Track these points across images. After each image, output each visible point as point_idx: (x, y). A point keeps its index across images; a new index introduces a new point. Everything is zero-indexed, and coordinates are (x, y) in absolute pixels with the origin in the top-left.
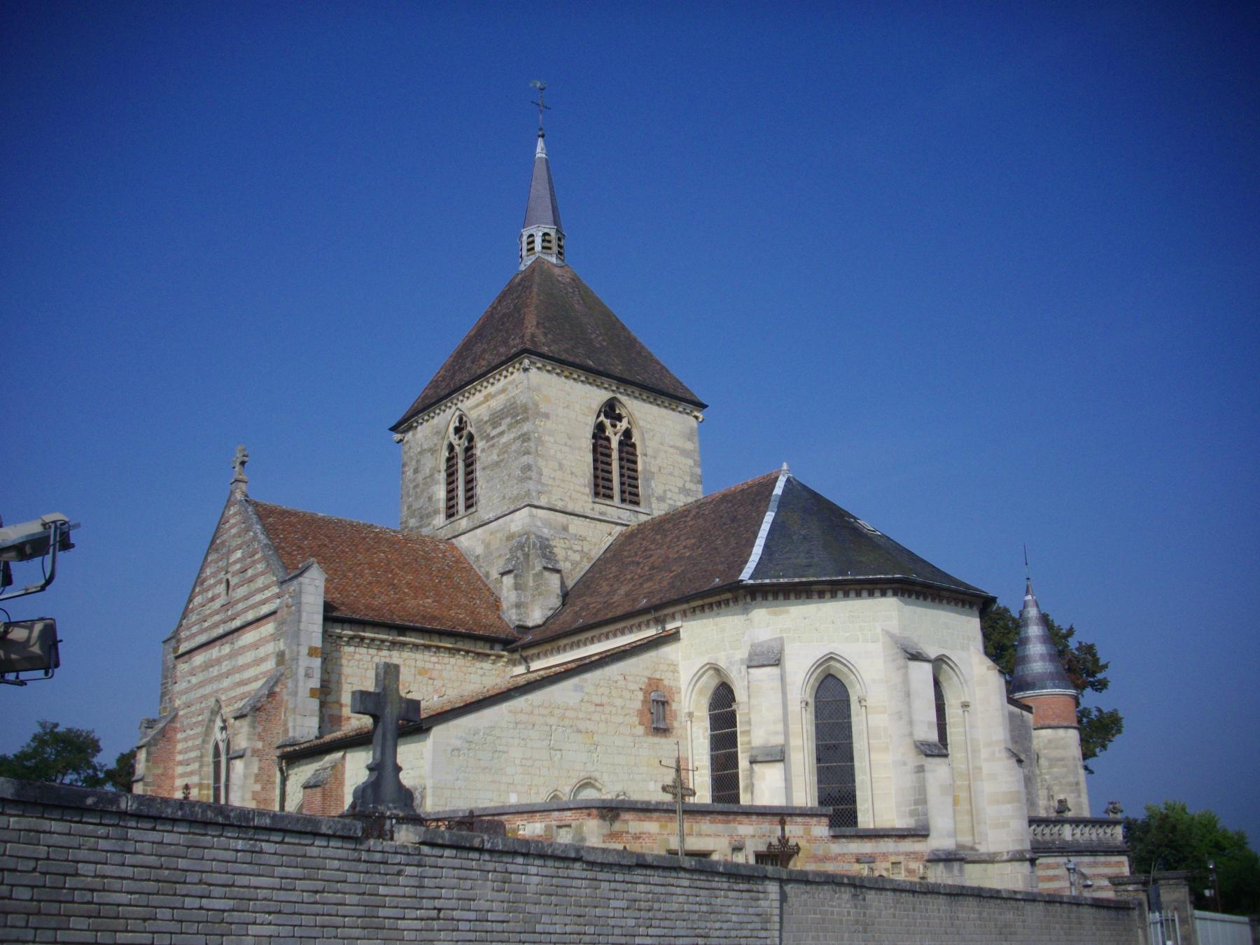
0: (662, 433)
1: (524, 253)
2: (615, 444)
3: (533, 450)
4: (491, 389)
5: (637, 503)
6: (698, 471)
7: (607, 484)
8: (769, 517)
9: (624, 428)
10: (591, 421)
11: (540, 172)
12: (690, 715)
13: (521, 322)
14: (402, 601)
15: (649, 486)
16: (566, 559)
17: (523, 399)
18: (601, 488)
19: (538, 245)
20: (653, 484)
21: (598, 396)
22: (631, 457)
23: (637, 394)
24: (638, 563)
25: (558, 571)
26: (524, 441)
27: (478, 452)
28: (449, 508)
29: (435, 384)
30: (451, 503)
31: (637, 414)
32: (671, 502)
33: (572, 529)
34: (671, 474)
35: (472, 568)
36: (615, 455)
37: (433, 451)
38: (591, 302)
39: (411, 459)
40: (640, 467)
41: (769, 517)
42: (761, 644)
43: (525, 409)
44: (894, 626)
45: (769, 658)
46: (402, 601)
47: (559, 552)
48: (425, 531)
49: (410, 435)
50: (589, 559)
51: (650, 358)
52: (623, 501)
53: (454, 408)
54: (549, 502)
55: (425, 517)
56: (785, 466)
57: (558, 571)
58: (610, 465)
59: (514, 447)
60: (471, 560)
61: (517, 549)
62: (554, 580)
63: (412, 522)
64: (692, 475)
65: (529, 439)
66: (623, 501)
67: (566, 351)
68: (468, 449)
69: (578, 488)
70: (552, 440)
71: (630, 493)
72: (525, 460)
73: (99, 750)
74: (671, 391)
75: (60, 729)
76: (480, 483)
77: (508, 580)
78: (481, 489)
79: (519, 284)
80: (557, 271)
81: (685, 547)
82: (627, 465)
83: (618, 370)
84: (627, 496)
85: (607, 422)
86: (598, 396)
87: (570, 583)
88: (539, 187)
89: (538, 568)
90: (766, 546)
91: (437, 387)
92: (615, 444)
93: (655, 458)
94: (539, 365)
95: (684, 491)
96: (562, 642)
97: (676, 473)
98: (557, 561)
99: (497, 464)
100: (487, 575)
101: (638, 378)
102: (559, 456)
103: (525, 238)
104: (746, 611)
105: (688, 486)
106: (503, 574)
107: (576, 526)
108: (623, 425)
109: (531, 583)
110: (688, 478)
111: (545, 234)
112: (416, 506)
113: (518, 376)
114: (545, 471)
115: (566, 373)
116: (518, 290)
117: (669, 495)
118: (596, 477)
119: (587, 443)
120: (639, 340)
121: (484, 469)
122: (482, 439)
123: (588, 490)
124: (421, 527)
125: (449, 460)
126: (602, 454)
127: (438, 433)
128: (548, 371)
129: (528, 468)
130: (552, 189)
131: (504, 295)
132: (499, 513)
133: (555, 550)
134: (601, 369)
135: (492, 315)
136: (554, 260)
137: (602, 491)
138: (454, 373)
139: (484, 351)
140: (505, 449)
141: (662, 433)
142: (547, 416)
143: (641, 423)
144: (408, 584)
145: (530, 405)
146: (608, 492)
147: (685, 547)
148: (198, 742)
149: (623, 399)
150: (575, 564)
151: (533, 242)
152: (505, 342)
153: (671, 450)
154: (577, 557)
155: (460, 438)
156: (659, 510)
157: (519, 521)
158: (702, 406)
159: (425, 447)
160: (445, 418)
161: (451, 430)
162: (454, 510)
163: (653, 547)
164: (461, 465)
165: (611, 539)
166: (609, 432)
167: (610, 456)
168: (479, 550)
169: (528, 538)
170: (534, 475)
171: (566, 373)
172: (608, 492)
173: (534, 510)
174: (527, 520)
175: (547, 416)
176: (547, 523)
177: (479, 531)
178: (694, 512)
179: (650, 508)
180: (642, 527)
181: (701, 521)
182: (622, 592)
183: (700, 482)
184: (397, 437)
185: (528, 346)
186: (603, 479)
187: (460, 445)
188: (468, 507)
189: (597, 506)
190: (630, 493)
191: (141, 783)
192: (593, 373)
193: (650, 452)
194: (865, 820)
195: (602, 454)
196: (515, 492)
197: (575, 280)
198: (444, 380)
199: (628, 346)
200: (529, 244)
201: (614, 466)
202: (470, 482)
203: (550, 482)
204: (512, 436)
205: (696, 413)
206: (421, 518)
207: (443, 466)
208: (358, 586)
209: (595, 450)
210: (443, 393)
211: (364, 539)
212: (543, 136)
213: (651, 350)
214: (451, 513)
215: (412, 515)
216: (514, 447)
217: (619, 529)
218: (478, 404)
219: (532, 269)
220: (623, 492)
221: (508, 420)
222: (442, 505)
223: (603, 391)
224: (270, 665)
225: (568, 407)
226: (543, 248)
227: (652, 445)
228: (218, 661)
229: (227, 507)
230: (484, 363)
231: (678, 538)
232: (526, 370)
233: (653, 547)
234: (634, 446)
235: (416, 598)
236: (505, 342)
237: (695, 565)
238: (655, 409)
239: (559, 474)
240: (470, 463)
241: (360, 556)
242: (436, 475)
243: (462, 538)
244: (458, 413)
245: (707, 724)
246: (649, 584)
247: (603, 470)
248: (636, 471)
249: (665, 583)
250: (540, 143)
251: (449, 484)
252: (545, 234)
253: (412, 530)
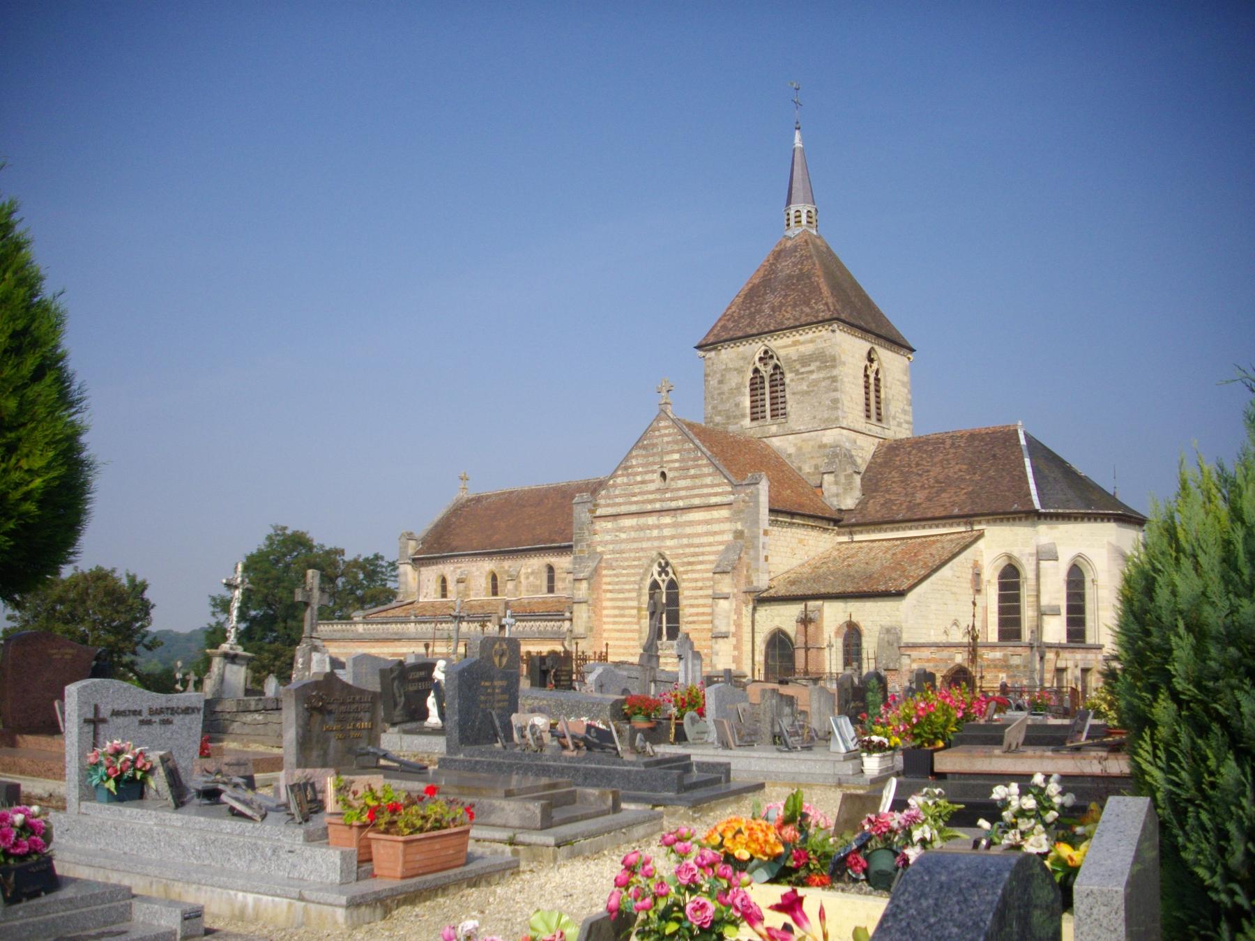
4: (801, 338)
8: (1027, 462)
12: (989, 581)
19: (804, 219)
31: (882, 358)
37: (740, 371)
39: (715, 372)
41: (1027, 462)
42: (1043, 546)
44: (1113, 540)
45: (1046, 554)
55: (731, 417)
56: (1020, 423)
59: (823, 384)
63: (718, 419)
73: (342, 552)
75: (289, 532)
90: (1036, 484)
96: (885, 526)
99: (807, 393)
104: (1034, 525)
122: (791, 372)
140: (815, 383)
148: (638, 578)
158: (912, 350)
161: (757, 359)
168: (791, 450)
176: (848, 439)
184: (701, 353)
187: (766, 371)
191: (584, 606)
194: (1090, 640)
196: (826, 416)
206: (728, 418)
217: (877, 440)
221: (818, 363)
224: (728, 537)
227: (889, 379)
228: (650, 528)
229: (658, 419)
232: (833, 331)
244: (763, 348)
245: (997, 587)
250: (797, 135)
253: (718, 424)
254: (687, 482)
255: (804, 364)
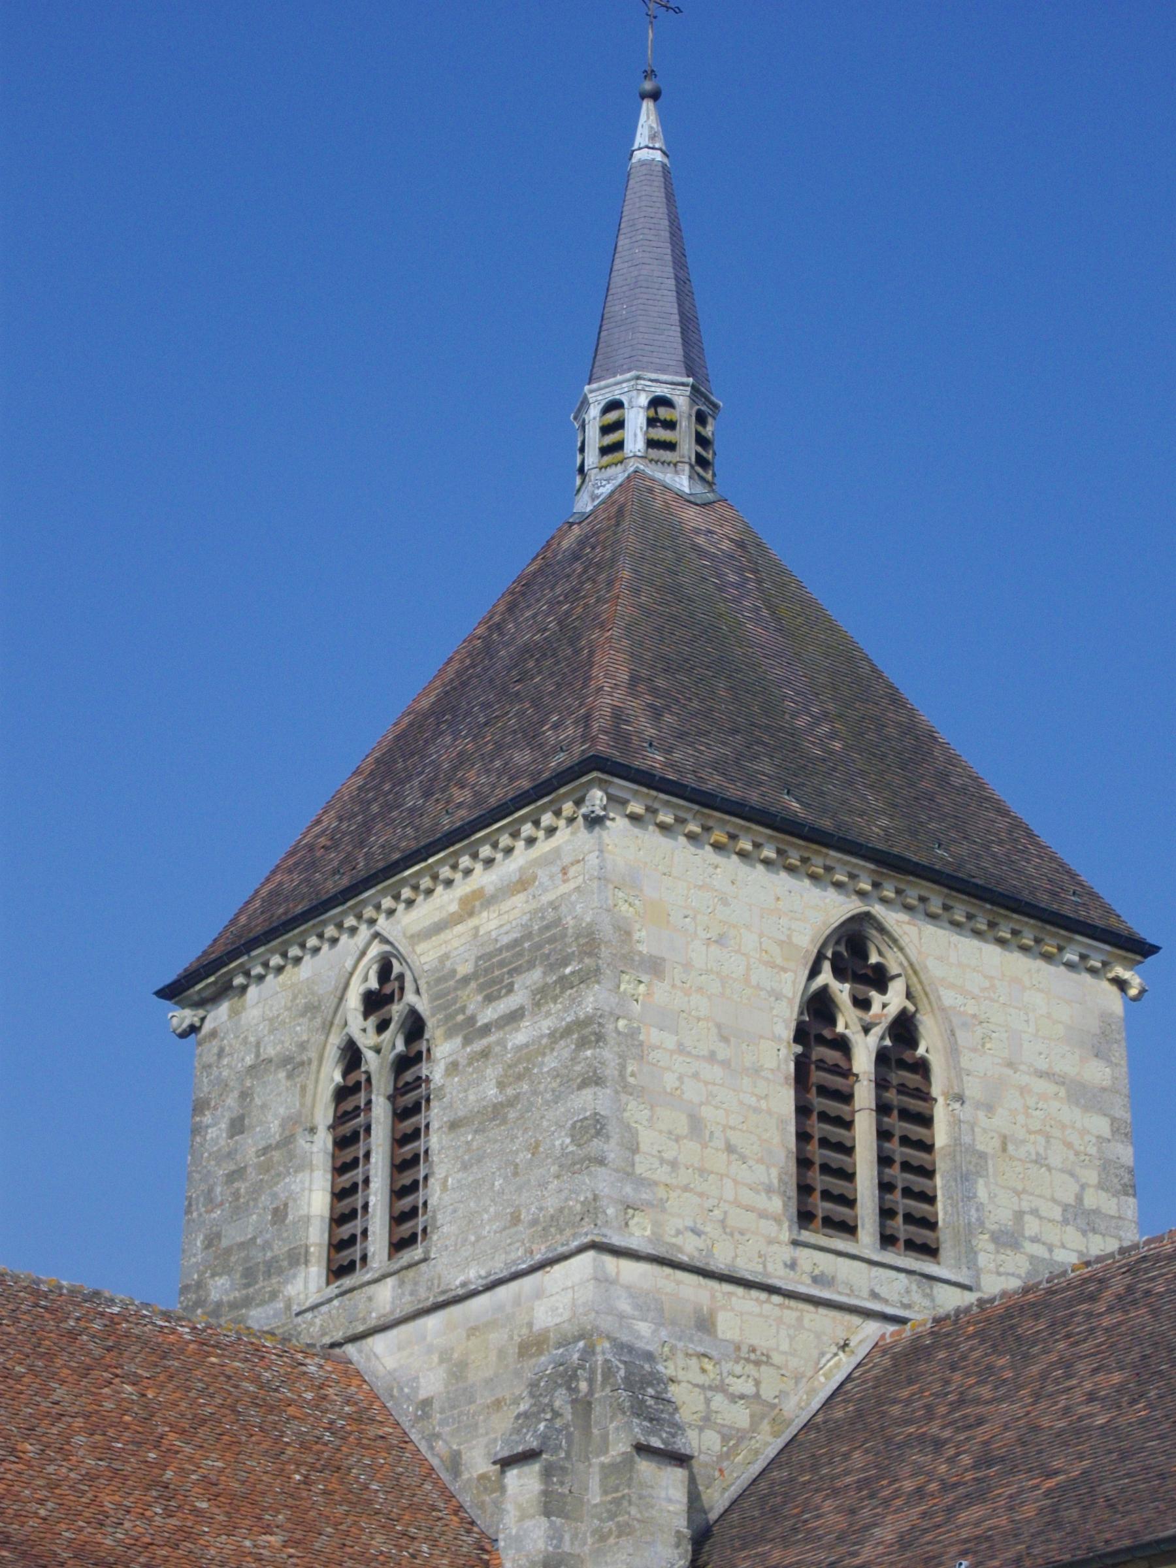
0: (1006, 1024)
1: (592, 458)
2: (863, 1061)
3: (611, 1071)
4: (483, 879)
5: (930, 1251)
6: (1125, 1153)
7: (837, 1185)
9: (893, 1011)
10: (790, 989)
11: (644, 207)
13: (579, 672)
14: (189, 1536)
15: (970, 1197)
16: (707, 1420)
17: (582, 913)
18: (819, 1198)
19: (635, 436)
20: (982, 1193)
21: (814, 908)
22: (914, 1105)
23: (935, 906)
24: (938, 1444)
25: (681, 1459)
26: (583, 1043)
27: (435, 1072)
28: (338, 1245)
29: (304, 858)
30: (345, 1231)
31: (934, 969)
32: (1038, 1250)
33: (727, 1327)
34: (1039, 1161)
35: (405, 1440)
36: (864, 1094)
38: (795, 614)
39: (225, 1086)
40: (941, 1136)
43: (590, 942)
46: (189, 1536)
47: (686, 1398)
48: (259, 1317)
49: (219, 1015)
50: (778, 1422)
51: (977, 794)
52: (887, 1240)
53: (364, 932)
54: (656, 1238)
55: (262, 1271)
57: (681, 1459)
58: (848, 1125)
59: (550, 1062)
60: (405, 1413)
61: (553, 1384)
62: (669, 1487)
63: (220, 1288)
64: (1106, 1166)
65: (600, 1038)
66: (887, 1240)
67: (718, 766)
68: (404, 1063)
69: (747, 1196)
70: (670, 1041)
71: (909, 1218)
72: (587, 1101)
74: (1044, 900)
76: (440, 1172)
77: (523, 1484)
78: (445, 1188)
79: (576, 556)
80: (691, 517)
81: (1091, 1397)
82: (901, 1127)
83: (875, 829)
84: (897, 1224)
85: (842, 992)
86: (814, 908)
87: (717, 1500)
88: (642, 256)
89: (620, 1447)
91: (313, 865)
92: (863, 1061)
93: (990, 1108)
94: (636, 807)
95: (1080, 1216)
97: (1055, 1160)
98: (678, 1428)
99: (497, 1112)
100: (455, 1463)
101: (941, 857)
102: (692, 1092)
103: (594, 412)
105: (1091, 1199)
106: (506, 1463)
107: (740, 1317)
108: (892, 1001)
109: (595, 1497)
110: (1091, 1176)
111: (657, 402)
112: (232, 1235)
113: (569, 839)
114: (646, 1138)
115: (719, 836)
116: (568, 574)
117: (1032, 1226)
118: (803, 1163)
119: (778, 1054)
120: (943, 736)
121: (454, 1126)
123: (779, 1206)
124: (247, 1302)
125: (342, 1094)
126: (823, 1091)
127: (311, 1009)
128: (663, 827)
129: (595, 1126)
130: (680, 261)
131: (522, 592)
132: (498, 1266)
133: (674, 1392)
134: (826, 824)
135: (488, 649)
136: (682, 482)
137: (822, 1207)
138: (367, 826)
139: (463, 760)
140: (522, 1067)
141: (1006, 1024)
142: (655, 966)
143: (949, 998)
144: (207, 1482)
145: (606, 930)
146: (841, 1211)
147: (1091, 1397)
149: (892, 918)
150: (733, 1438)
151: (619, 425)
152: (531, 736)
153: (1041, 1085)
154: (739, 1416)
155: (382, 1027)
156: (1000, 1276)
157: (562, 1296)
158: (1139, 949)
159: (270, 1051)
160: (337, 965)
161: (354, 1001)
162: (356, 1252)
163: (985, 1392)
164: (381, 1113)
165: (846, 1363)
166: (847, 1021)
167: (847, 1098)
168: (432, 1384)
169: (589, 1352)
170: (612, 1150)
171: (719, 836)
172: (841, 1211)
173: (609, 1261)
174: (588, 1293)
175: (655, 966)
176: (650, 1306)
177: (432, 1322)
178: (1118, 1285)
179: (972, 1264)
180: (946, 1329)
181: (1140, 1314)
182: (886, 1533)
183: (1131, 1189)
184: (183, 1017)
185: (604, 746)
186: (826, 1169)
187: (380, 1051)
188: (398, 1245)
189: (803, 1254)
190: (909, 1218)
192: (801, 836)
193: (973, 1089)
195: (823, 1091)
196: (552, 1204)
197: (748, 546)
198: (335, 845)
199: (907, 751)
200: (606, 430)
201: (861, 1130)
202: (408, 1167)
203: (662, 1174)
204: (546, 1025)
205: (1120, 971)
206: (249, 1275)
207: (324, 1114)
208: (53, 1485)
209: (801, 1078)
210: (332, 886)
211: (73, 1335)
212: (655, 96)
213: (981, 769)
214: (343, 1260)
215: (221, 1262)
216: (550, 1062)
217: (872, 1330)
218: (440, 924)
219: (615, 509)
220: (886, 1213)
221: (535, 976)
222: (317, 1236)
223: (832, 894)
225: (720, 941)
226: (652, 444)
230: (461, 796)
231: (1067, 1365)
233: (985, 1392)
234: (922, 1068)
235: (230, 1529)
236: (531, 736)
237: (1124, 1456)
238: (991, 952)
239: (689, 1151)
240: (409, 1106)
241: (60, 1393)
242: (301, 1142)
243: (379, 1344)
244: (376, 949)
246: (976, 1512)
247: (824, 1143)
248: (928, 1148)
249: (1029, 1511)
250: (648, 117)
251: (340, 1169)
252: (657, 402)
253: (216, 1311)
254: (13, 1459)
255: (494, 989)
